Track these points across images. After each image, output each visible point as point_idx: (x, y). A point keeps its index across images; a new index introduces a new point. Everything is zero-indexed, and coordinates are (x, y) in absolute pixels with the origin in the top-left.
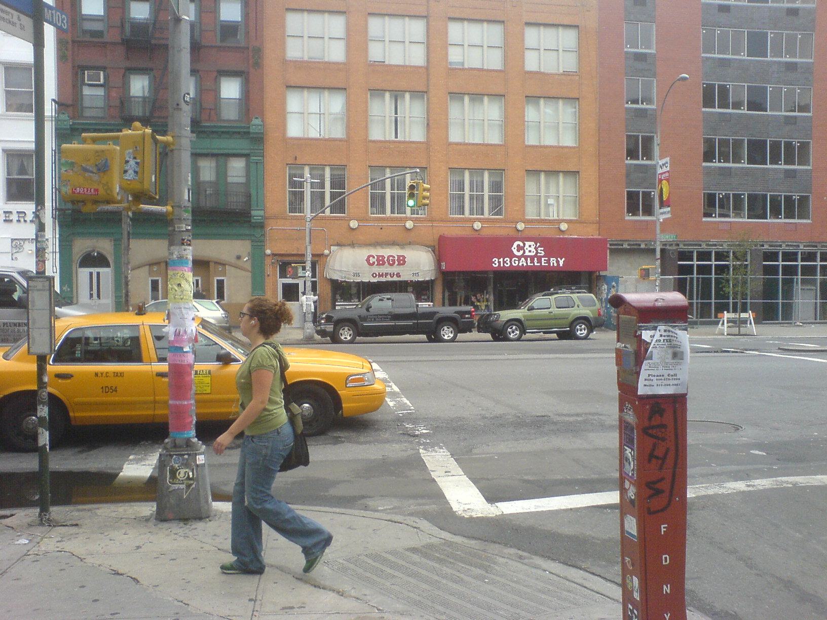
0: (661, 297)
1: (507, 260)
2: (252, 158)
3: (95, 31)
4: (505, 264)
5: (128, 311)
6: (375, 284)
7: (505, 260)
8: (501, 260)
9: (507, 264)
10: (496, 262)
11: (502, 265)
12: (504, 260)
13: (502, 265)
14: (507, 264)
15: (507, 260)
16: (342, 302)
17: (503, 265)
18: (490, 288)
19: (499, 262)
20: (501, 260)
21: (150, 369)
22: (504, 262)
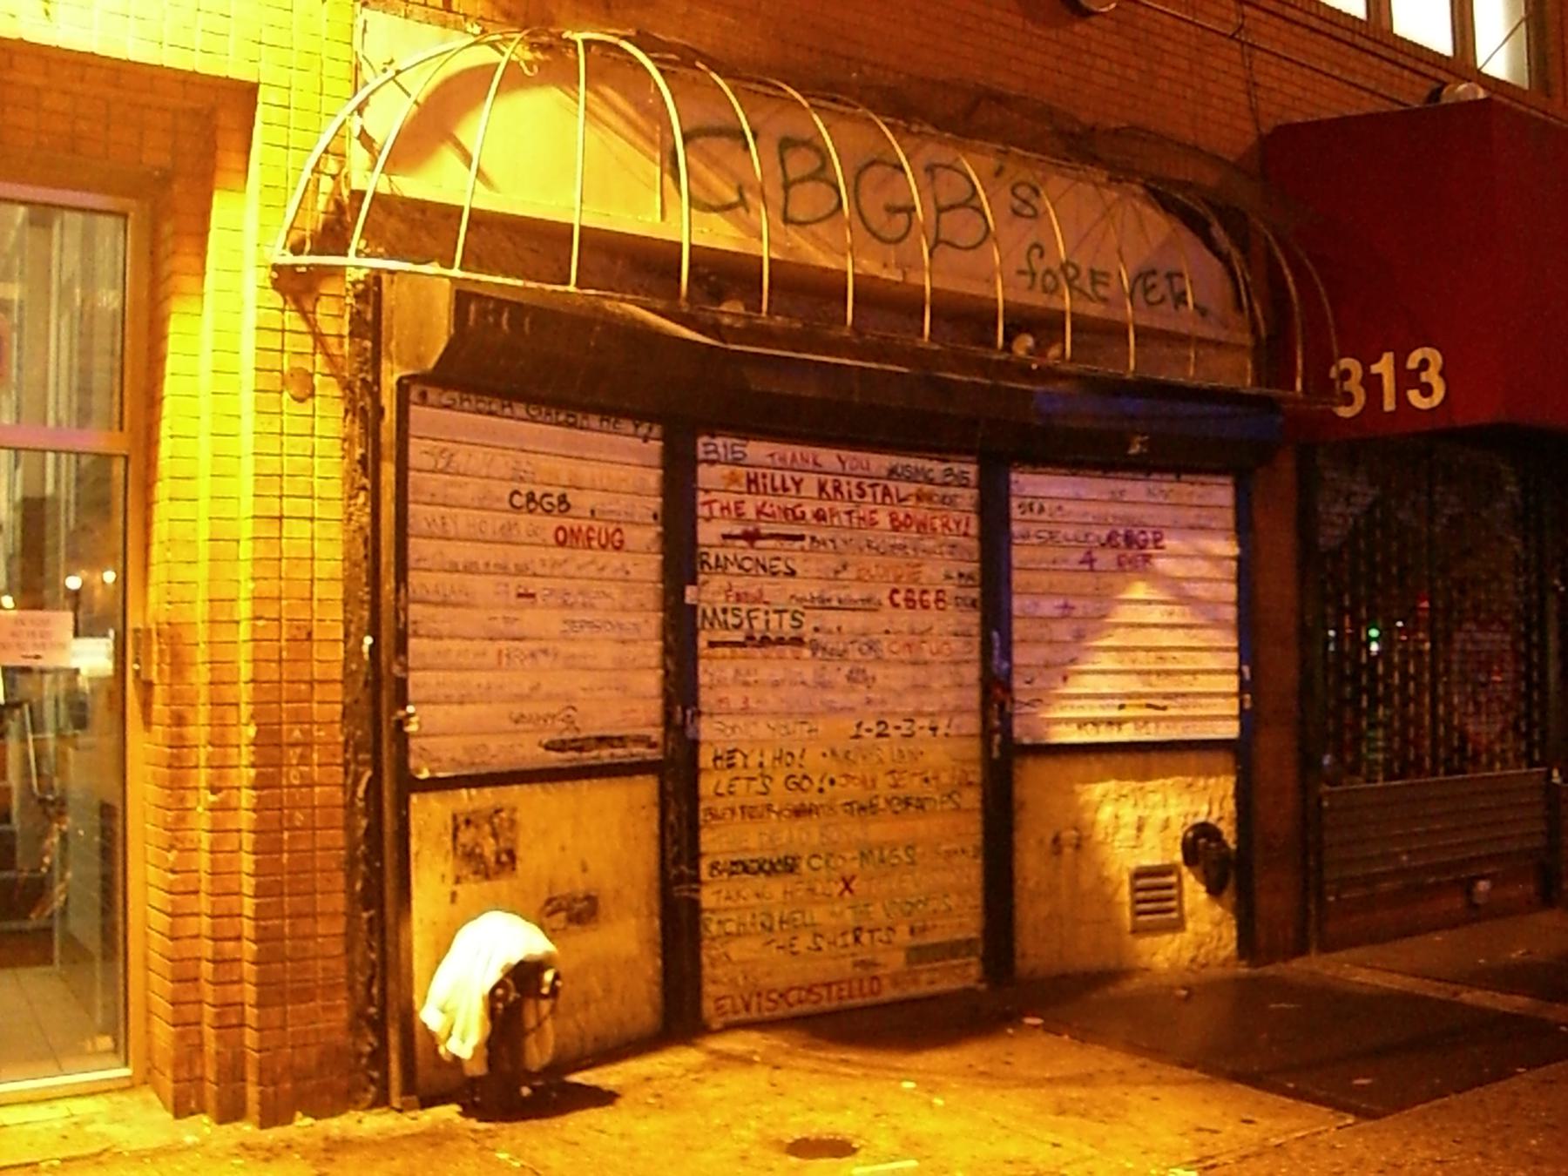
0: (448, 839)
1: (1424, 364)
2: (50, 489)
3: (1193, 230)
4: (1414, 396)
5: (47, 960)
6: (1205, 872)
7: (1413, 362)
8: (1384, 367)
9: (1427, 390)
10: (1354, 386)
11: (1389, 405)
12: (1399, 365)
13: (1389, 405)
14: (1427, 390)
15: (1424, 364)
16: (380, 256)
17: (1401, 398)
18: (1243, 970)
19: (1373, 384)
20: (1384, 367)
21: (278, 465)
22: (1408, 379)
